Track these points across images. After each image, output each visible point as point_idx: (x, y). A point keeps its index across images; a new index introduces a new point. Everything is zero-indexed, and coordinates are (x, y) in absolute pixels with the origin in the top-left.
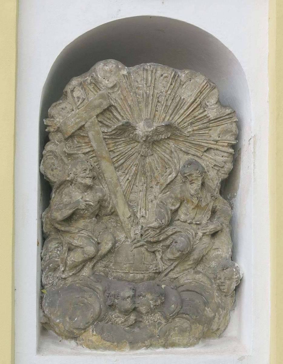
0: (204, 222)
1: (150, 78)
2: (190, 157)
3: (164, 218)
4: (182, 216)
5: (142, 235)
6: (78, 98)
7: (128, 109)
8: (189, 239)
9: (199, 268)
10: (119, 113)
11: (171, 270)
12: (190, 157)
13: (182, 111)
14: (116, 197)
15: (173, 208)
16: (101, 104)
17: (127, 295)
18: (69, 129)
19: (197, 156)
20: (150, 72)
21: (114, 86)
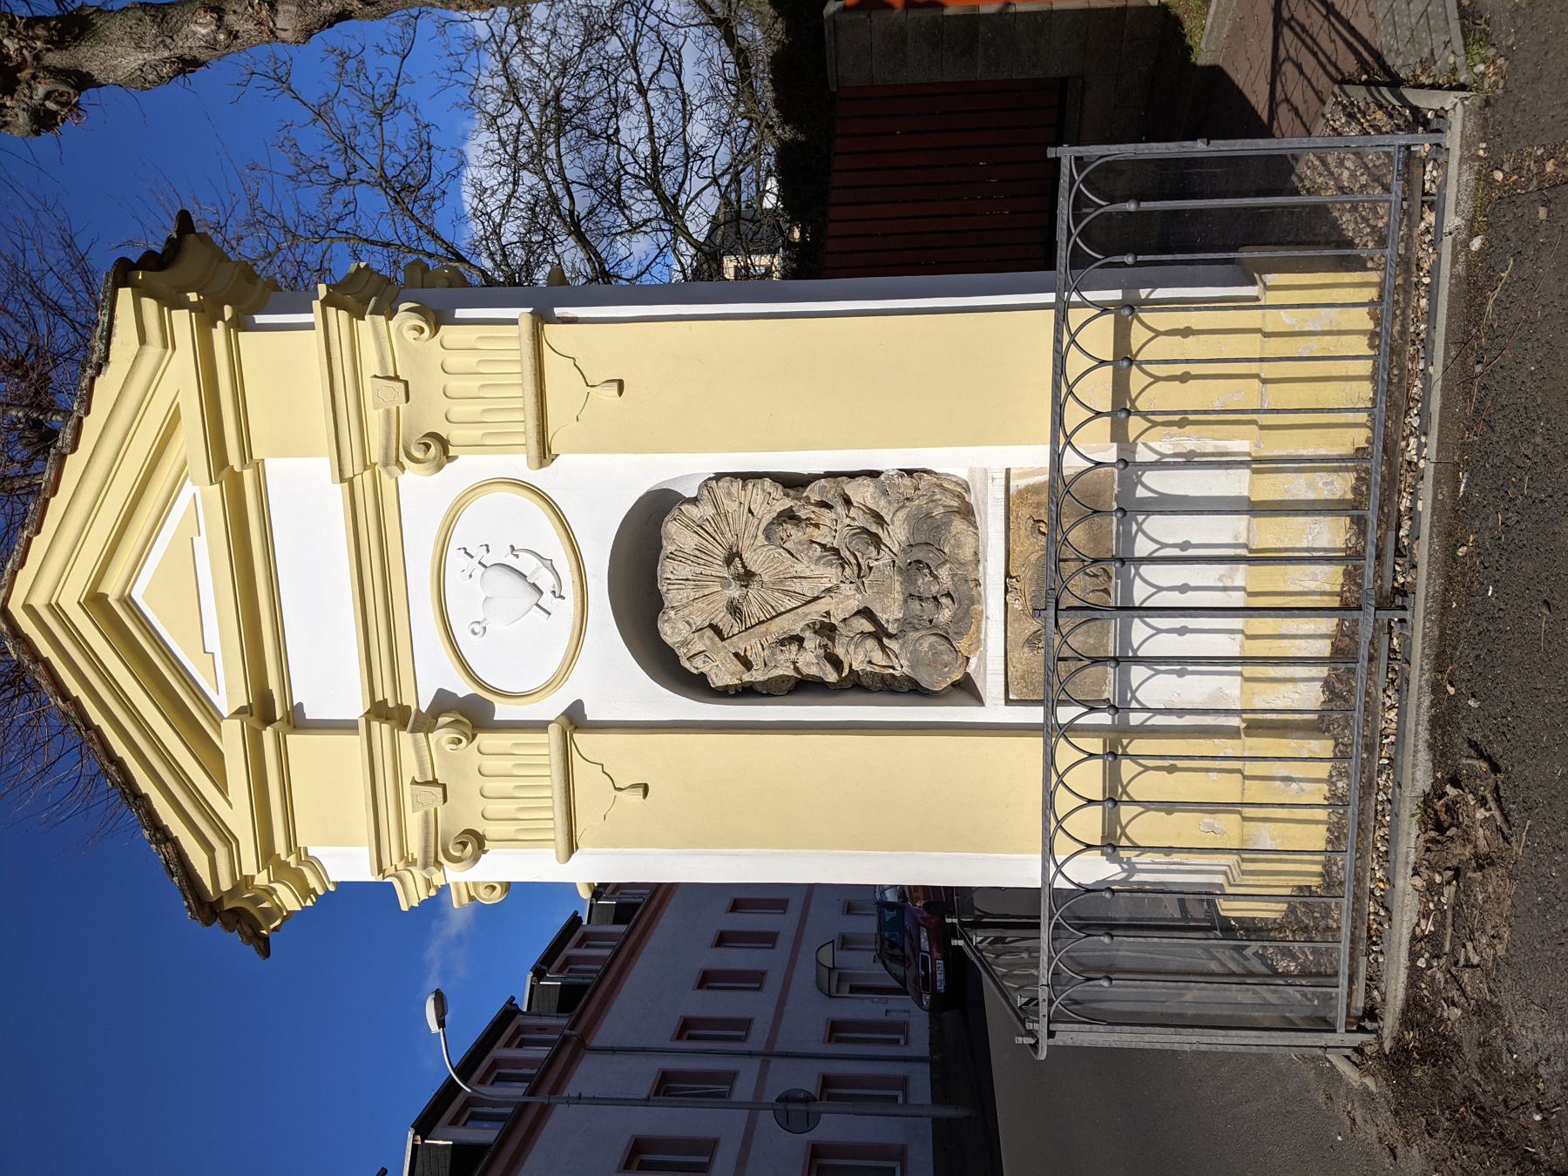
0: (834, 516)
1: (676, 586)
2: (760, 533)
3: (831, 560)
4: (826, 541)
5: (851, 583)
6: (704, 662)
7: (712, 605)
8: (854, 535)
9: (887, 519)
10: (716, 616)
11: (890, 550)
12: (760, 533)
13: (710, 547)
14: (810, 614)
15: (819, 549)
16: (708, 637)
17: (919, 607)
18: (469, 173)
19: (759, 524)
20: (670, 587)
21: (688, 623)
